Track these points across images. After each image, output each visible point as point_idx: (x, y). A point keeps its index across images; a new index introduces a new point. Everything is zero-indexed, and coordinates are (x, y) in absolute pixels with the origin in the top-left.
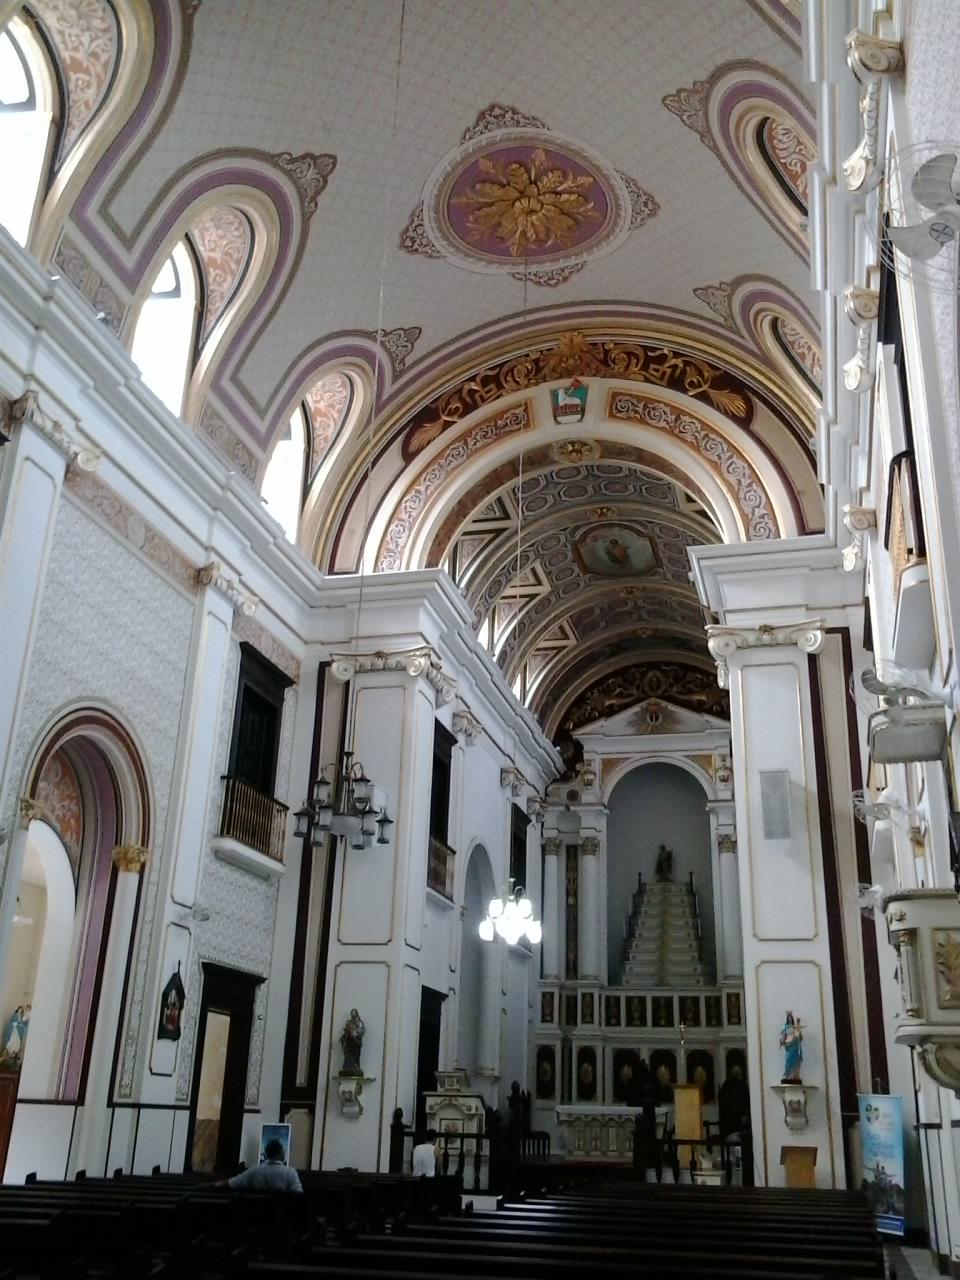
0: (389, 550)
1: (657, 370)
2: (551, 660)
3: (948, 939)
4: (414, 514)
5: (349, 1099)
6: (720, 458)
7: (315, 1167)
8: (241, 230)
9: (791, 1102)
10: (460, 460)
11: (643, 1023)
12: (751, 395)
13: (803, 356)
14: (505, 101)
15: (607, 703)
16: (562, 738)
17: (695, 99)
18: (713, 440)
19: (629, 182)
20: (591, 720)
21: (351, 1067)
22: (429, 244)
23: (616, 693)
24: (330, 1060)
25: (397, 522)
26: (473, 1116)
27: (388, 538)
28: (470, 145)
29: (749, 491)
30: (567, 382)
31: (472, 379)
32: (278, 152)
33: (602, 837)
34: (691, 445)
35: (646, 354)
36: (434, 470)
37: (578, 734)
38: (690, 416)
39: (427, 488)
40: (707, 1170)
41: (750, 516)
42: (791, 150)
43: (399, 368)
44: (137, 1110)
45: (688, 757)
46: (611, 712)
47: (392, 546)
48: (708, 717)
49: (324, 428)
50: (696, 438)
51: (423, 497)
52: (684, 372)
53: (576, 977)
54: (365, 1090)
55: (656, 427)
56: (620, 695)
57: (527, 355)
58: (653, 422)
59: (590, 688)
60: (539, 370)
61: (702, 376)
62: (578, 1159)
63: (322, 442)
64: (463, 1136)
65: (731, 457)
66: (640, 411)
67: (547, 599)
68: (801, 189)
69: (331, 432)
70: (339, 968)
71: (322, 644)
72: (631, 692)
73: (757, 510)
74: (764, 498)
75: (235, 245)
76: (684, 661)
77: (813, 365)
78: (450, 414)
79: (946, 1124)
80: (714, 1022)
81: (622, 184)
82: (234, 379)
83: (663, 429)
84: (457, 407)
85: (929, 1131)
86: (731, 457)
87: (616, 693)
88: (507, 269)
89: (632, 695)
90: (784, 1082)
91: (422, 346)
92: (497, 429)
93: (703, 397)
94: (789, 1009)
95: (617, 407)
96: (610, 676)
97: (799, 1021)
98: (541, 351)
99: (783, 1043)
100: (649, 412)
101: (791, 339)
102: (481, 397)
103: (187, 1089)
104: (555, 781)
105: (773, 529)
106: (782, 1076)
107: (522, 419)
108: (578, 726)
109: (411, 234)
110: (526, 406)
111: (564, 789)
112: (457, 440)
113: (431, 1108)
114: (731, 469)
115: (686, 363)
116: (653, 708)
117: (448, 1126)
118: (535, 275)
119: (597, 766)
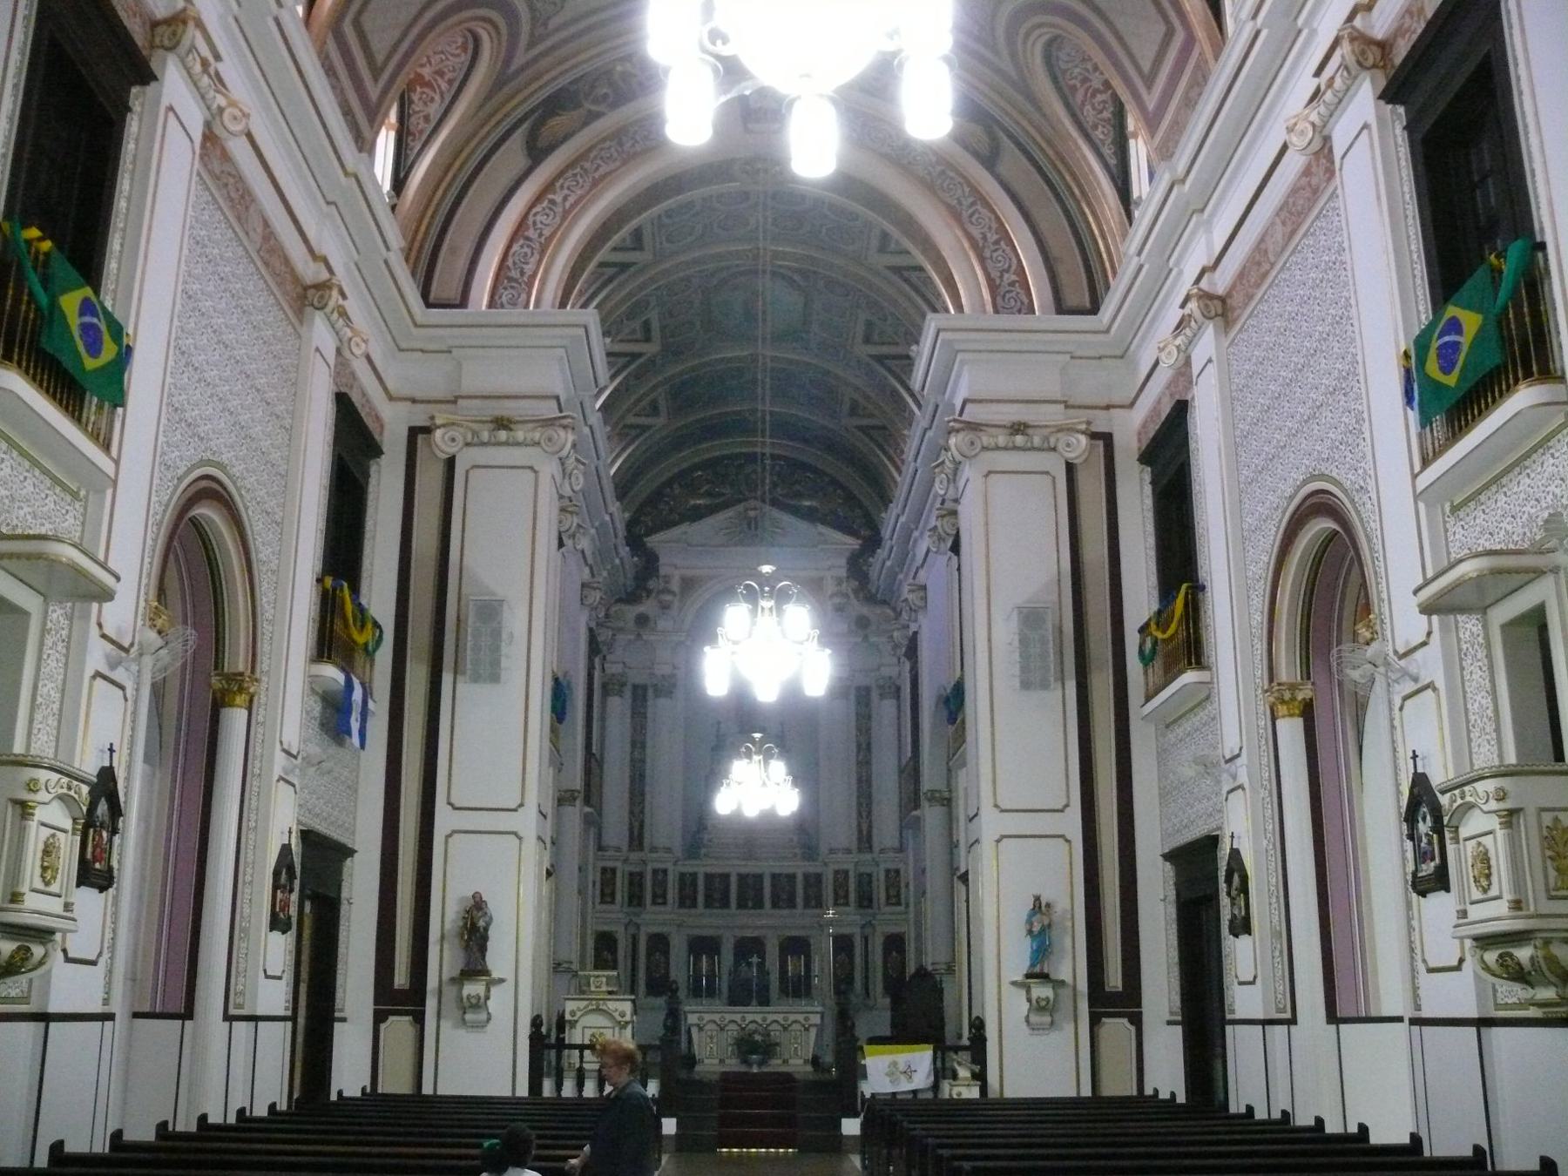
0: (510, 279)
2: (633, 441)
3: (1556, 819)
4: (547, 232)
5: (479, 1004)
6: (960, 203)
7: (427, 1089)
9: (469, 997)
10: (612, 166)
11: (759, 904)
13: (1074, 89)
15: (692, 502)
16: (635, 541)
20: (668, 525)
21: (474, 968)
23: (702, 491)
24: (442, 960)
25: (521, 242)
26: (627, 1023)
27: (510, 262)
29: (996, 250)
37: (653, 541)
39: (565, 199)
40: (966, 1079)
41: (998, 282)
44: (42, 1025)
46: (697, 515)
47: (514, 274)
49: (425, 103)
51: (559, 210)
53: (641, 847)
54: (494, 990)
56: (709, 494)
59: (669, 483)
63: (421, 121)
65: (973, 204)
67: (652, 361)
69: (435, 110)
70: (450, 840)
71: (414, 401)
72: (724, 491)
73: (1006, 276)
74: (1014, 261)
79: (1407, 1021)
80: (688, 902)
82: (357, 24)
85: (1484, 1030)
87: (702, 491)
90: (1028, 976)
94: (1037, 892)
96: (696, 467)
99: (1030, 932)
101: (1063, 66)
104: (619, 601)
105: (1026, 301)
106: (1024, 967)
108: (651, 531)
111: (631, 611)
113: (573, 1013)
114: (973, 220)
116: (752, 514)
117: (593, 1035)
119: (675, 586)
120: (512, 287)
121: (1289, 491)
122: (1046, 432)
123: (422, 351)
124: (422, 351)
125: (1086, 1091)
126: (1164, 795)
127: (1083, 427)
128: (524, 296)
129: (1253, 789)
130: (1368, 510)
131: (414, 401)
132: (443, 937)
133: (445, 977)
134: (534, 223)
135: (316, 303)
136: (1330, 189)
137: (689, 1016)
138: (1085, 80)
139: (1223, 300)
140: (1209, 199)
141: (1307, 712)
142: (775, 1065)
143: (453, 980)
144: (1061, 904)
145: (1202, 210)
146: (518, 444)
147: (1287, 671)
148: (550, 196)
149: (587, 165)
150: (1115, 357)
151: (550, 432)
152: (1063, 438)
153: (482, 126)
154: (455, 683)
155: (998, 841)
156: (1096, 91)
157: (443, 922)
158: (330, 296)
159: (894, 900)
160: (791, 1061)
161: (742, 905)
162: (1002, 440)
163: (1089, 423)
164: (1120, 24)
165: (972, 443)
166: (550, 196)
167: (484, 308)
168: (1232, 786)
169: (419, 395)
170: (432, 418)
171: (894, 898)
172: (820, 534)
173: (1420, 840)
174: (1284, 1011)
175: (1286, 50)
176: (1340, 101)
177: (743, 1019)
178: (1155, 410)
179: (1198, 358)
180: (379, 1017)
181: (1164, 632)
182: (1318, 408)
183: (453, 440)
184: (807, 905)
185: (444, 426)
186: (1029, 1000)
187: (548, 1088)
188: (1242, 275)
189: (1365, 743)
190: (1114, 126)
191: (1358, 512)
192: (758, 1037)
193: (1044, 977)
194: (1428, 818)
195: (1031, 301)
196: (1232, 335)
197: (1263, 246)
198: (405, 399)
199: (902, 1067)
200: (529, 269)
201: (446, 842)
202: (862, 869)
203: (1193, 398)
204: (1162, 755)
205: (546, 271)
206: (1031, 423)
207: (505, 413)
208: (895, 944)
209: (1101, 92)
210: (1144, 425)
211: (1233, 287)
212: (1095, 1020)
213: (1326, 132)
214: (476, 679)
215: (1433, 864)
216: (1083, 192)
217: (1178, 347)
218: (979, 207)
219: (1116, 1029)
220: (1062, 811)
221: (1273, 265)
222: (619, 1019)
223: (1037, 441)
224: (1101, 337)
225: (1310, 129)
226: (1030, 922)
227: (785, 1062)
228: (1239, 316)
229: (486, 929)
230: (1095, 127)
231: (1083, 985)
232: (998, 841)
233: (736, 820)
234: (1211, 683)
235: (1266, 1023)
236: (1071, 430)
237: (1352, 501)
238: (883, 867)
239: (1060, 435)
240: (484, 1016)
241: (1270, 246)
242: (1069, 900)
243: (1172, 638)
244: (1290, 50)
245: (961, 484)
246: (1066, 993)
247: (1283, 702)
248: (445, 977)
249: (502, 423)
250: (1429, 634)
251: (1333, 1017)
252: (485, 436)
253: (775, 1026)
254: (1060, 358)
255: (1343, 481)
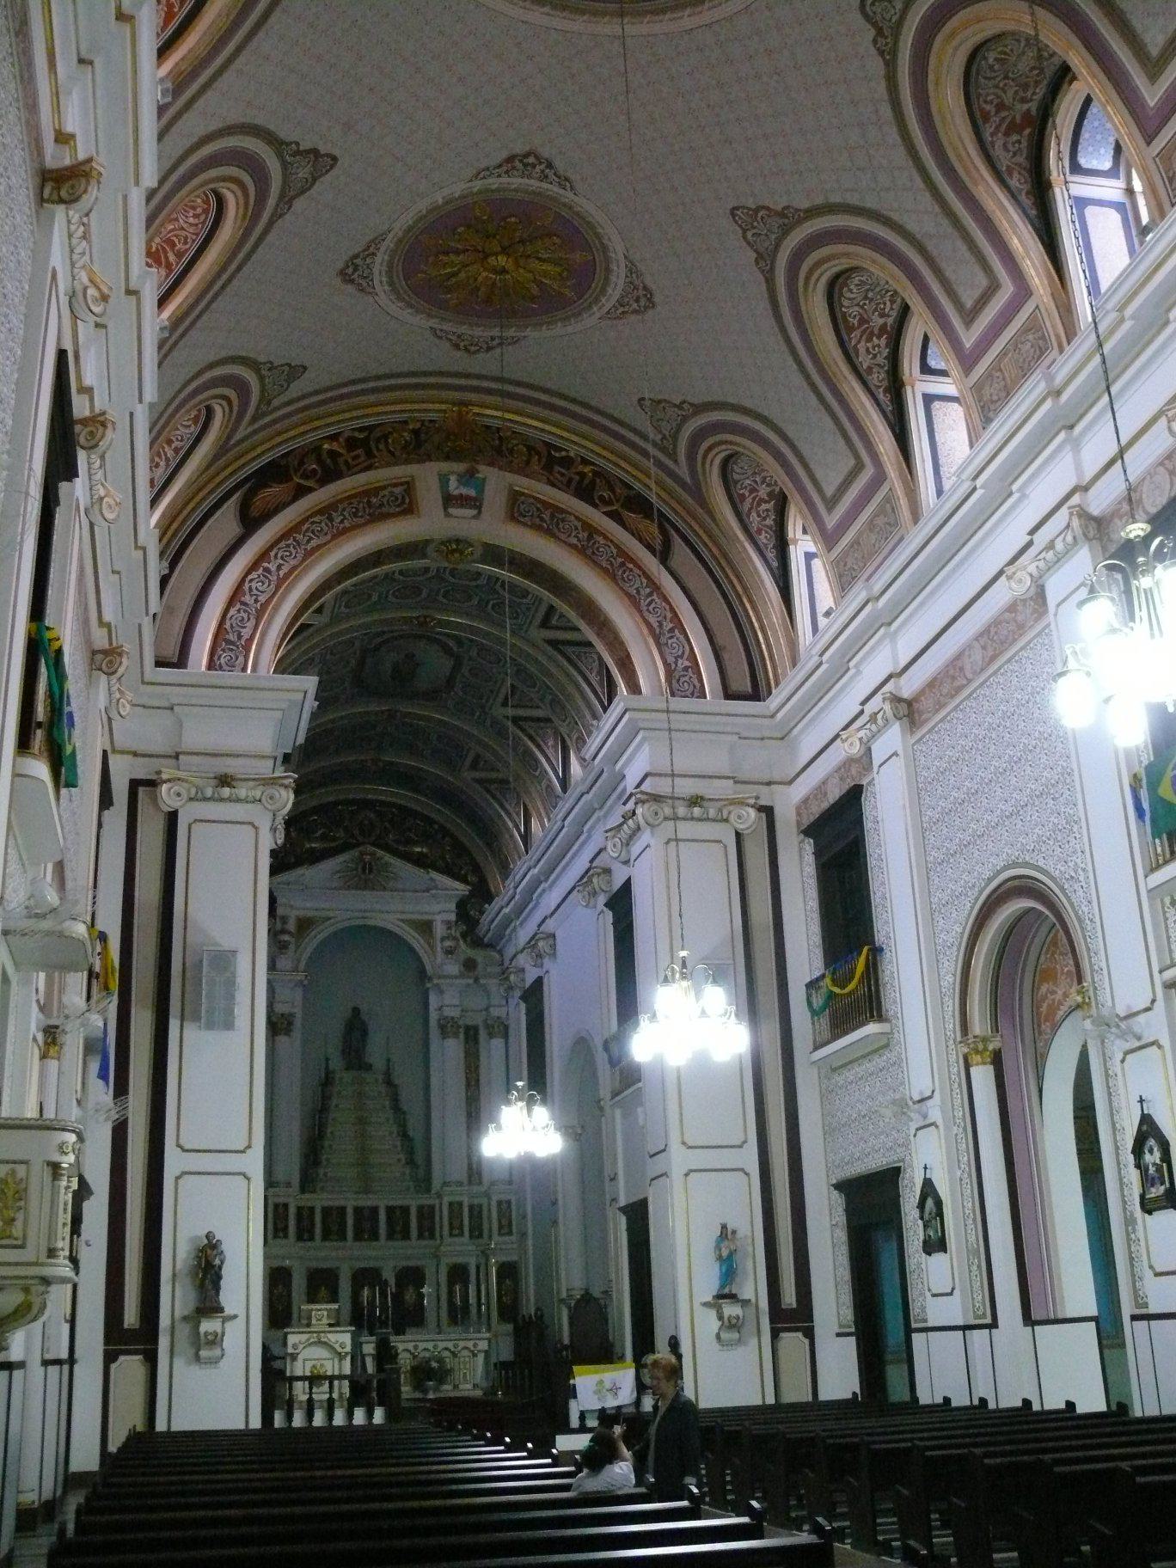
0: (229, 642)
1: (563, 475)
4: (262, 599)
5: (215, 1340)
6: (638, 592)
7: (161, 1426)
8: (202, 218)
9: (206, 1334)
11: (375, 1236)
12: (673, 532)
14: (545, 152)
17: (775, 223)
18: (631, 570)
19: (632, 269)
21: (208, 1303)
22: (368, 278)
23: (318, 835)
24: (174, 1300)
25: (238, 606)
27: (227, 626)
28: (478, 185)
29: (672, 637)
30: (461, 467)
31: (333, 438)
32: (288, 139)
33: (298, 1012)
34: (606, 571)
35: (550, 454)
36: (288, 546)
38: (606, 538)
39: (279, 567)
41: (673, 666)
42: (855, 302)
43: (264, 408)
45: (402, 920)
47: (232, 637)
48: (434, 875)
50: (612, 564)
52: (593, 483)
55: (565, 542)
56: (324, 838)
57: (406, 422)
58: (563, 537)
60: (419, 445)
61: (613, 491)
62: (466, 1394)
64: (331, 1379)
65: (650, 594)
66: (548, 521)
68: (853, 343)
71: (135, 754)
74: (687, 648)
75: (183, 233)
76: (361, 796)
77: (750, 509)
78: (306, 476)
81: (623, 272)
83: (571, 546)
84: (314, 470)
86: (650, 594)
87: (318, 835)
88: (433, 323)
89: (334, 839)
91: (295, 390)
92: (370, 507)
93: (614, 516)
95: (519, 509)
97: (734, 1232)
98: (423, 421)
100: (558, 524)
101: (736, 477)
102: (346, 462)
103: (981, 1297)
105: (698, 685)
107: (406, 504)
109: (358, 261)
110: (409, 486)
112: (320, 512)
113: (295, 1346)
114: (651, 608)
115: (596, 474)
116: (367, 858)
117: (314, 1366)
118: (459, 336)
120: (232, 650)
121: (987, 874)
122: (719, 804)
123: (144, 707)
124: (144, 707)
125: (771, 1400)
126: (829, 1132)
127: (752, 801)
128: (241, 659)
129: (947, 1128)
130: (1078, 897)
131: (135, 754)
132: (174, 1275)
133: (178, 1314)
134: (250, 589)
135: (104, 666)
136: (1039, 628)
137: (365, 1346)
138: (753, 490)
139: (909, 703)
140: (897, 617)
141: (997, 1060)
142: (447, 1390)
143: (185, 1319)
144: (743, 1230)
145: (890, 624)
146: (238, 800)
147: (979, 1024)
148: (266, 565)
149: (299, 537)
150: (776, 739)
151: (271, 791)
152: (736, 810)
153: (200, 490)
154: (182, 1026)
155: (686, 1175)
156: (762, 501)
157: (174, 1260)
158: (121, 663)
159: (505, 1230)
160: (461, 1387)
161: (358, 1237)
162: (682, 811)
163: (757, 798)
164: (802, 446)
165: (656, 814)
166: (266, 565)
167: (203, 669)
168: (923, 1124)
169: (141, 748)
170: (159, 773)
171: (506, 1228)
172: (432, 879)
173: (1147, 1169)
174: (984, 1316)
175: (997, 504)
176: (1059, 560)
177: (416, 1347)
178: (821, 789)
179: (879, 751)
180: (110, 1358)
181: (843, 987)
182: (1022, 807)
183: (179, 795)
184: (420, 1236)
185: (169, 780)
186: (720, 1318)
187: (278, 1419)
188: (932, 684)
189: (1045, 1087)
190: (775, 532)
191: (1068, 898)
192: (434, 1365)
193: (732, 1297)
194: (1155, 1149)
195: (703, 685)
196: (918, 735)
197: (959, 664)
198: (128, 753)
199: (608, 1385)
200: (246, 633)
201: (176, 1184)
202: (476, 1201)
203: (871, 783)
204: (826, 1095)
205: (263, 635)
206: (707, 797)
207: (230, 771)
208: (509, 1272)
209: (766, 502)
210: (806, 801)
211: (922, 692)
212: (775, 1335)
213: (1040, 582)
214: (210, 1026)
215: (1163, 1188)
216: (745, 589)
217: (861, 739)
218: (655, 597)
219: (793, 1341)
220: (740, 1147)
221: (970, 681)
222: (339, 1350)
223: (712, 813)
224: (766, 722)
225: (1029, 578)
226: (718, 1247)
227: (456, 1387)
228: (926, 720)
229: (220, 1268)
230: (759, 531)
231: (764, 1304)
232: (686, 1175)
233: (496, 1161)
234: (892, 1033)
235: (965, 1328)
236: (742, 803)
237: (1063, 889)
238: (446, 1200)
239: (731, 808)
240: (218, 1352)
241: (967, 663)
242: (750, 1227)
243: (850, 994)
244: (1001, 505)
245: (636, 849)
246: (751, 1311)
247: (977, 1052)
248: (178, 1314)
249: (225, 780)
250: (1153, 1001)
251: (1028, 1320)
252: (209, 792)
253: (446, 1354)
254: (729, 738)
255: (1052, 870)
